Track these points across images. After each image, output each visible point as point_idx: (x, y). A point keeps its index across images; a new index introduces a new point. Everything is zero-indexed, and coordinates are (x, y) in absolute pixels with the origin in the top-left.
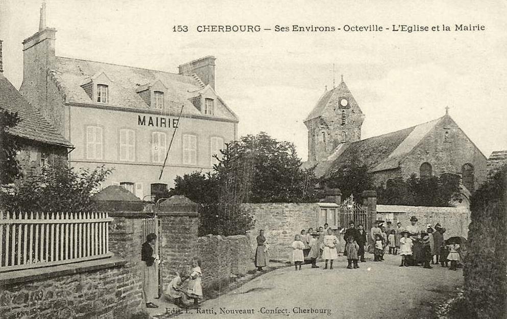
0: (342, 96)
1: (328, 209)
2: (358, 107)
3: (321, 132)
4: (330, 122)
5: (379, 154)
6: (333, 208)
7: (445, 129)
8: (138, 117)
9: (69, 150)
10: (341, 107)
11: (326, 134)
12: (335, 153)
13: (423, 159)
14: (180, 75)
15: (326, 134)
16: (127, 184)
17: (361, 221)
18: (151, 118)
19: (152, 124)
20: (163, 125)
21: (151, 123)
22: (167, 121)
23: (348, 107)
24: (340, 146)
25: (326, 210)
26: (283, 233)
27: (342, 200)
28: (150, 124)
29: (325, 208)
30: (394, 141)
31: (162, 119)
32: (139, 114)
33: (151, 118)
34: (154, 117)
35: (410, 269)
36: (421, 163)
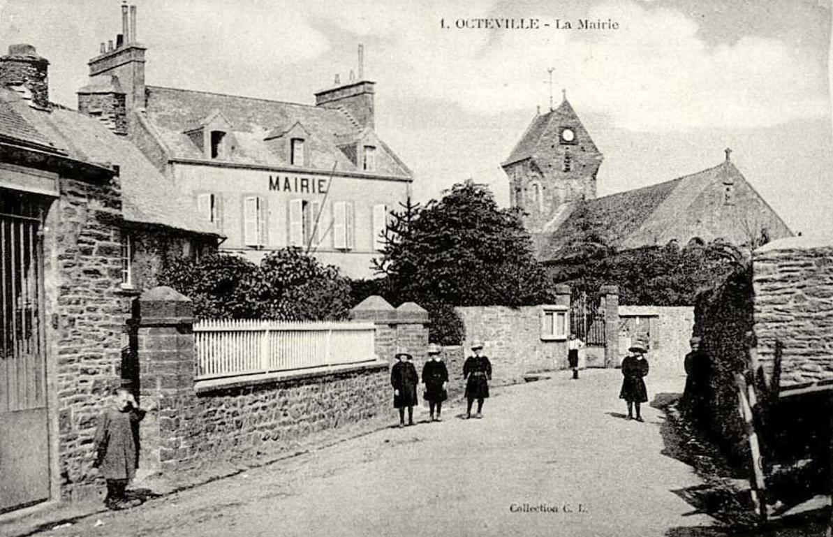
0: (563, 124)
1: (555, 314)
2: (591, 142)
3: (531, 184)
4: (546, 167)
5: (626, 223)
6: (561, 313)
7: (725, 184)
8: (268, 178)
9: (220, 240)
10: (563, 142)
11: (540, 187)
12: (555, 218)
13: (692, 232)
14: (318, 108)
15: (540, 187)
16: (38, 230)
17: (228, 345)
18: (287, 180)
19: (289, 187)
20: (305, 189)
21: (287, 187)
22: (310, 183)
23: (573, 143)
24: (563, 207)
25: (552, 314)
26: (498, 344)
27: (572, 302)
28: (285, 188)
29: (549, 313)
30: (654, 196)
31: (303, 180)
32: (271, 173)
33: (287, 180)
34: (291, 177)
35: (529, 314)
36: (690, 238)
